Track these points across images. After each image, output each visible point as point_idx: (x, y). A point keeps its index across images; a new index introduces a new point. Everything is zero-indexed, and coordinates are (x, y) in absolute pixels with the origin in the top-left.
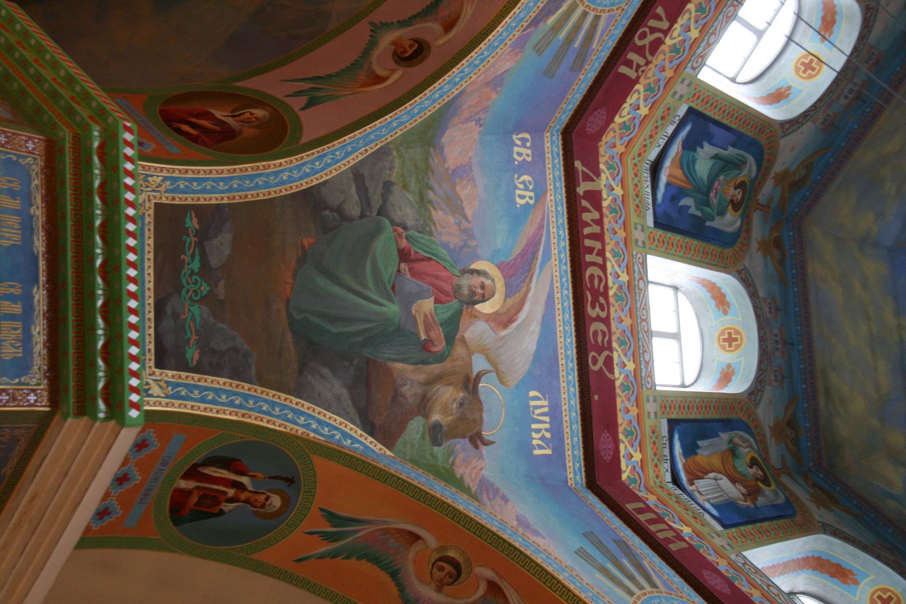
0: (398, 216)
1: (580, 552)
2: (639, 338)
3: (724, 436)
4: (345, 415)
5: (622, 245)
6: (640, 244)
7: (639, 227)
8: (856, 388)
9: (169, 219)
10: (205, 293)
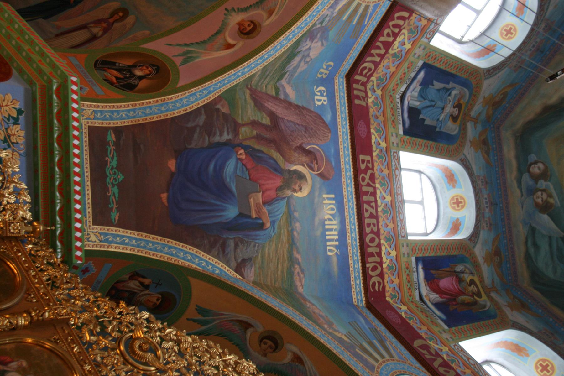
2: (396, 207)
5: (382, 125)
6: (395, 145)
7: (394, 135)
9: (97, 136)
10: (121, 179)
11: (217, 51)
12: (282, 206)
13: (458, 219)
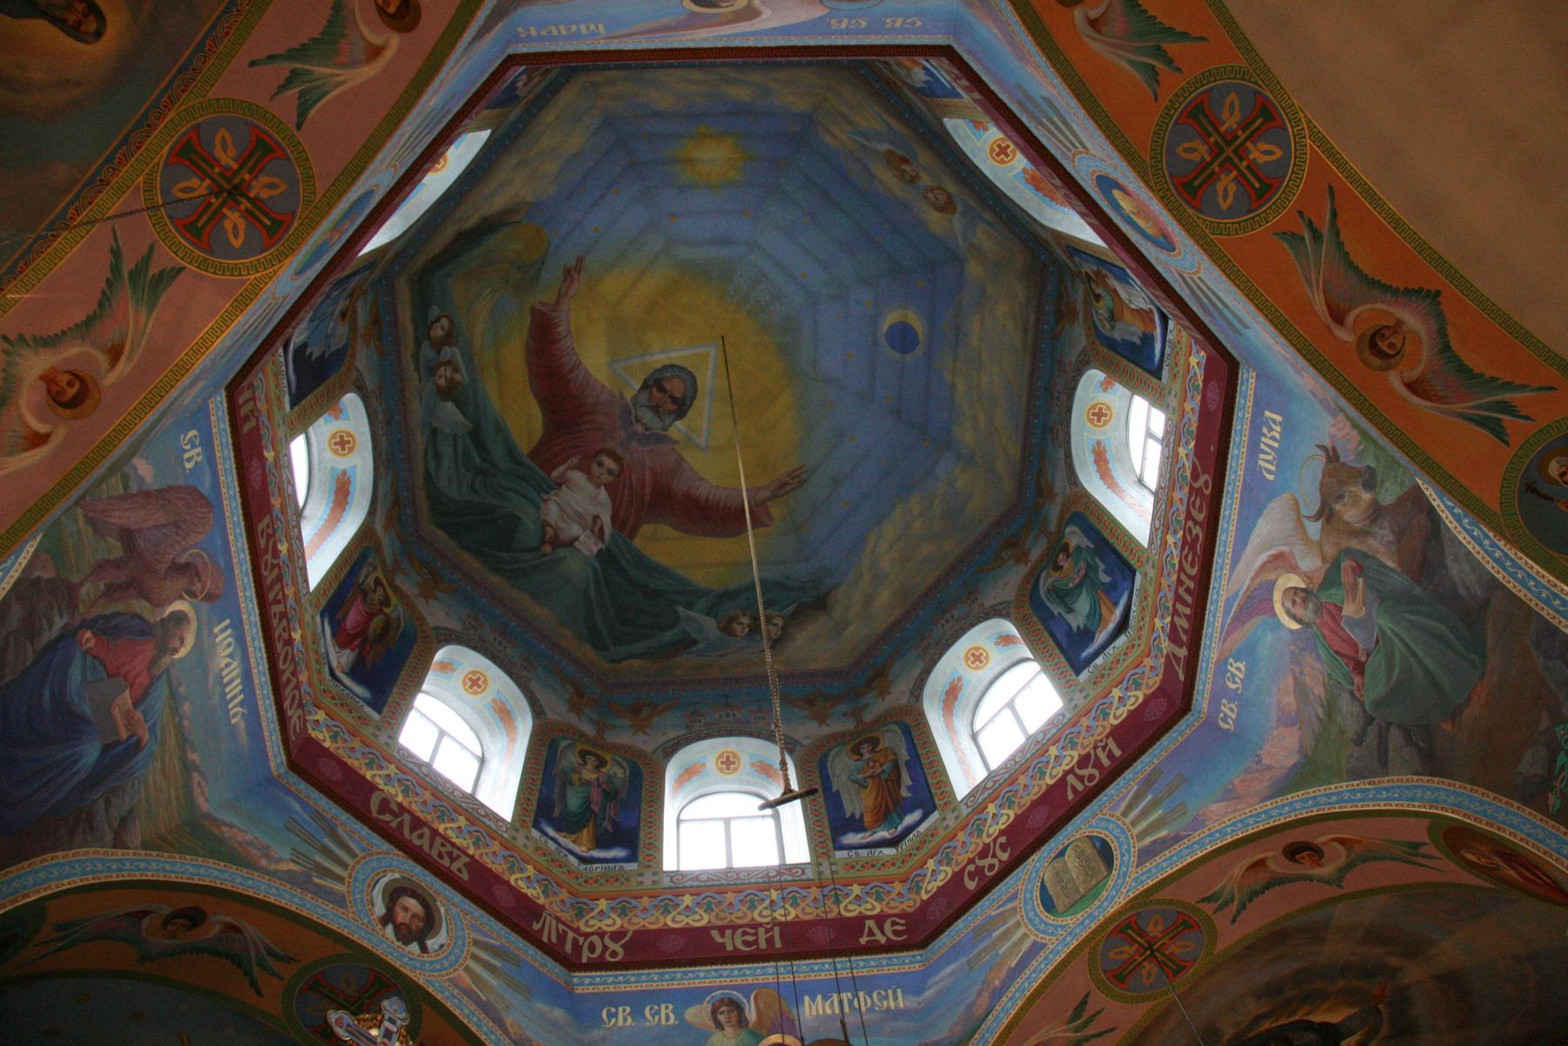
0: (1356, 708)
1: (1247, 327)
3: (1117, 335)
4: (1454, 539)
8: (996, 325)
11: (10, 454)
12: (162, 690)
13: (344, 473)
